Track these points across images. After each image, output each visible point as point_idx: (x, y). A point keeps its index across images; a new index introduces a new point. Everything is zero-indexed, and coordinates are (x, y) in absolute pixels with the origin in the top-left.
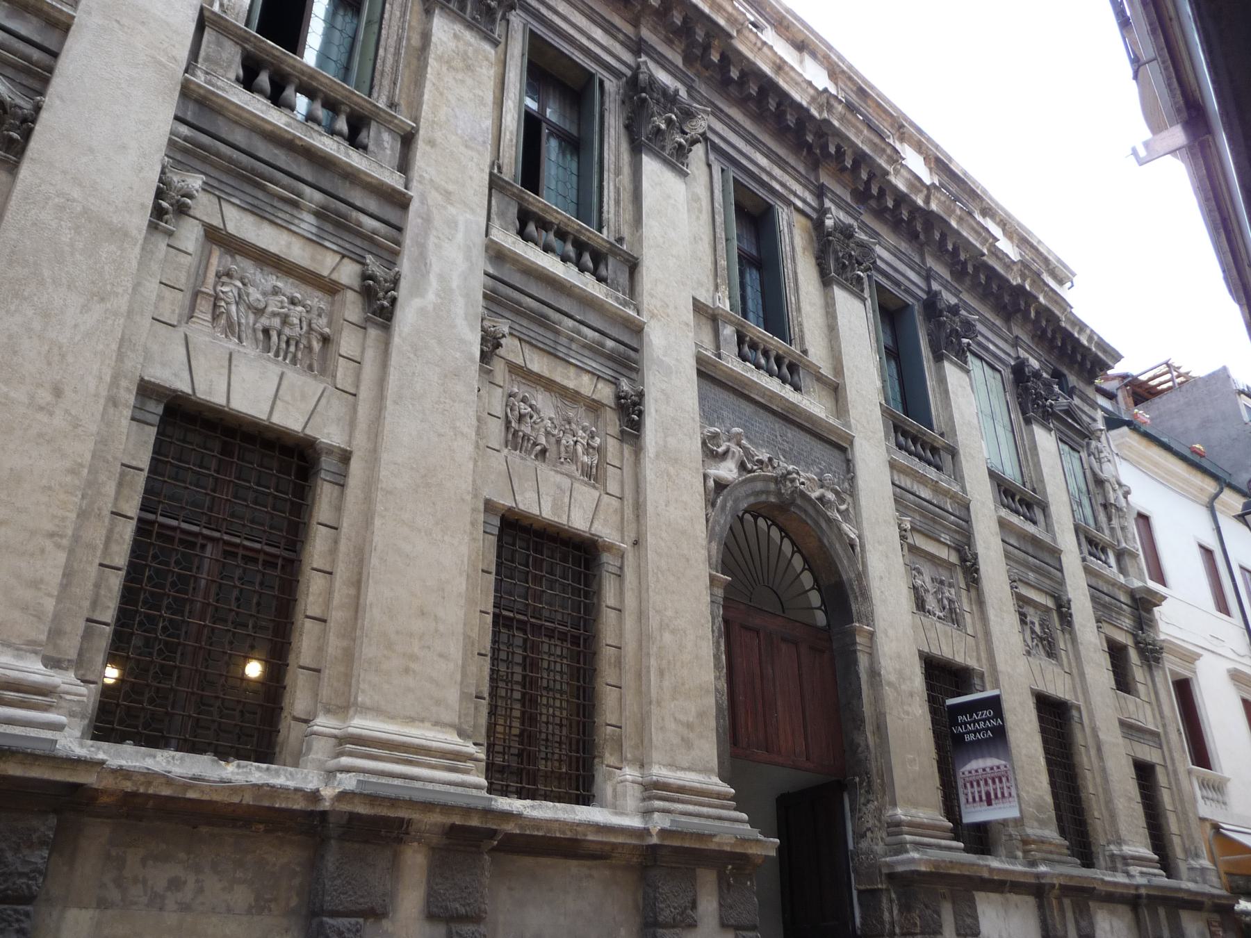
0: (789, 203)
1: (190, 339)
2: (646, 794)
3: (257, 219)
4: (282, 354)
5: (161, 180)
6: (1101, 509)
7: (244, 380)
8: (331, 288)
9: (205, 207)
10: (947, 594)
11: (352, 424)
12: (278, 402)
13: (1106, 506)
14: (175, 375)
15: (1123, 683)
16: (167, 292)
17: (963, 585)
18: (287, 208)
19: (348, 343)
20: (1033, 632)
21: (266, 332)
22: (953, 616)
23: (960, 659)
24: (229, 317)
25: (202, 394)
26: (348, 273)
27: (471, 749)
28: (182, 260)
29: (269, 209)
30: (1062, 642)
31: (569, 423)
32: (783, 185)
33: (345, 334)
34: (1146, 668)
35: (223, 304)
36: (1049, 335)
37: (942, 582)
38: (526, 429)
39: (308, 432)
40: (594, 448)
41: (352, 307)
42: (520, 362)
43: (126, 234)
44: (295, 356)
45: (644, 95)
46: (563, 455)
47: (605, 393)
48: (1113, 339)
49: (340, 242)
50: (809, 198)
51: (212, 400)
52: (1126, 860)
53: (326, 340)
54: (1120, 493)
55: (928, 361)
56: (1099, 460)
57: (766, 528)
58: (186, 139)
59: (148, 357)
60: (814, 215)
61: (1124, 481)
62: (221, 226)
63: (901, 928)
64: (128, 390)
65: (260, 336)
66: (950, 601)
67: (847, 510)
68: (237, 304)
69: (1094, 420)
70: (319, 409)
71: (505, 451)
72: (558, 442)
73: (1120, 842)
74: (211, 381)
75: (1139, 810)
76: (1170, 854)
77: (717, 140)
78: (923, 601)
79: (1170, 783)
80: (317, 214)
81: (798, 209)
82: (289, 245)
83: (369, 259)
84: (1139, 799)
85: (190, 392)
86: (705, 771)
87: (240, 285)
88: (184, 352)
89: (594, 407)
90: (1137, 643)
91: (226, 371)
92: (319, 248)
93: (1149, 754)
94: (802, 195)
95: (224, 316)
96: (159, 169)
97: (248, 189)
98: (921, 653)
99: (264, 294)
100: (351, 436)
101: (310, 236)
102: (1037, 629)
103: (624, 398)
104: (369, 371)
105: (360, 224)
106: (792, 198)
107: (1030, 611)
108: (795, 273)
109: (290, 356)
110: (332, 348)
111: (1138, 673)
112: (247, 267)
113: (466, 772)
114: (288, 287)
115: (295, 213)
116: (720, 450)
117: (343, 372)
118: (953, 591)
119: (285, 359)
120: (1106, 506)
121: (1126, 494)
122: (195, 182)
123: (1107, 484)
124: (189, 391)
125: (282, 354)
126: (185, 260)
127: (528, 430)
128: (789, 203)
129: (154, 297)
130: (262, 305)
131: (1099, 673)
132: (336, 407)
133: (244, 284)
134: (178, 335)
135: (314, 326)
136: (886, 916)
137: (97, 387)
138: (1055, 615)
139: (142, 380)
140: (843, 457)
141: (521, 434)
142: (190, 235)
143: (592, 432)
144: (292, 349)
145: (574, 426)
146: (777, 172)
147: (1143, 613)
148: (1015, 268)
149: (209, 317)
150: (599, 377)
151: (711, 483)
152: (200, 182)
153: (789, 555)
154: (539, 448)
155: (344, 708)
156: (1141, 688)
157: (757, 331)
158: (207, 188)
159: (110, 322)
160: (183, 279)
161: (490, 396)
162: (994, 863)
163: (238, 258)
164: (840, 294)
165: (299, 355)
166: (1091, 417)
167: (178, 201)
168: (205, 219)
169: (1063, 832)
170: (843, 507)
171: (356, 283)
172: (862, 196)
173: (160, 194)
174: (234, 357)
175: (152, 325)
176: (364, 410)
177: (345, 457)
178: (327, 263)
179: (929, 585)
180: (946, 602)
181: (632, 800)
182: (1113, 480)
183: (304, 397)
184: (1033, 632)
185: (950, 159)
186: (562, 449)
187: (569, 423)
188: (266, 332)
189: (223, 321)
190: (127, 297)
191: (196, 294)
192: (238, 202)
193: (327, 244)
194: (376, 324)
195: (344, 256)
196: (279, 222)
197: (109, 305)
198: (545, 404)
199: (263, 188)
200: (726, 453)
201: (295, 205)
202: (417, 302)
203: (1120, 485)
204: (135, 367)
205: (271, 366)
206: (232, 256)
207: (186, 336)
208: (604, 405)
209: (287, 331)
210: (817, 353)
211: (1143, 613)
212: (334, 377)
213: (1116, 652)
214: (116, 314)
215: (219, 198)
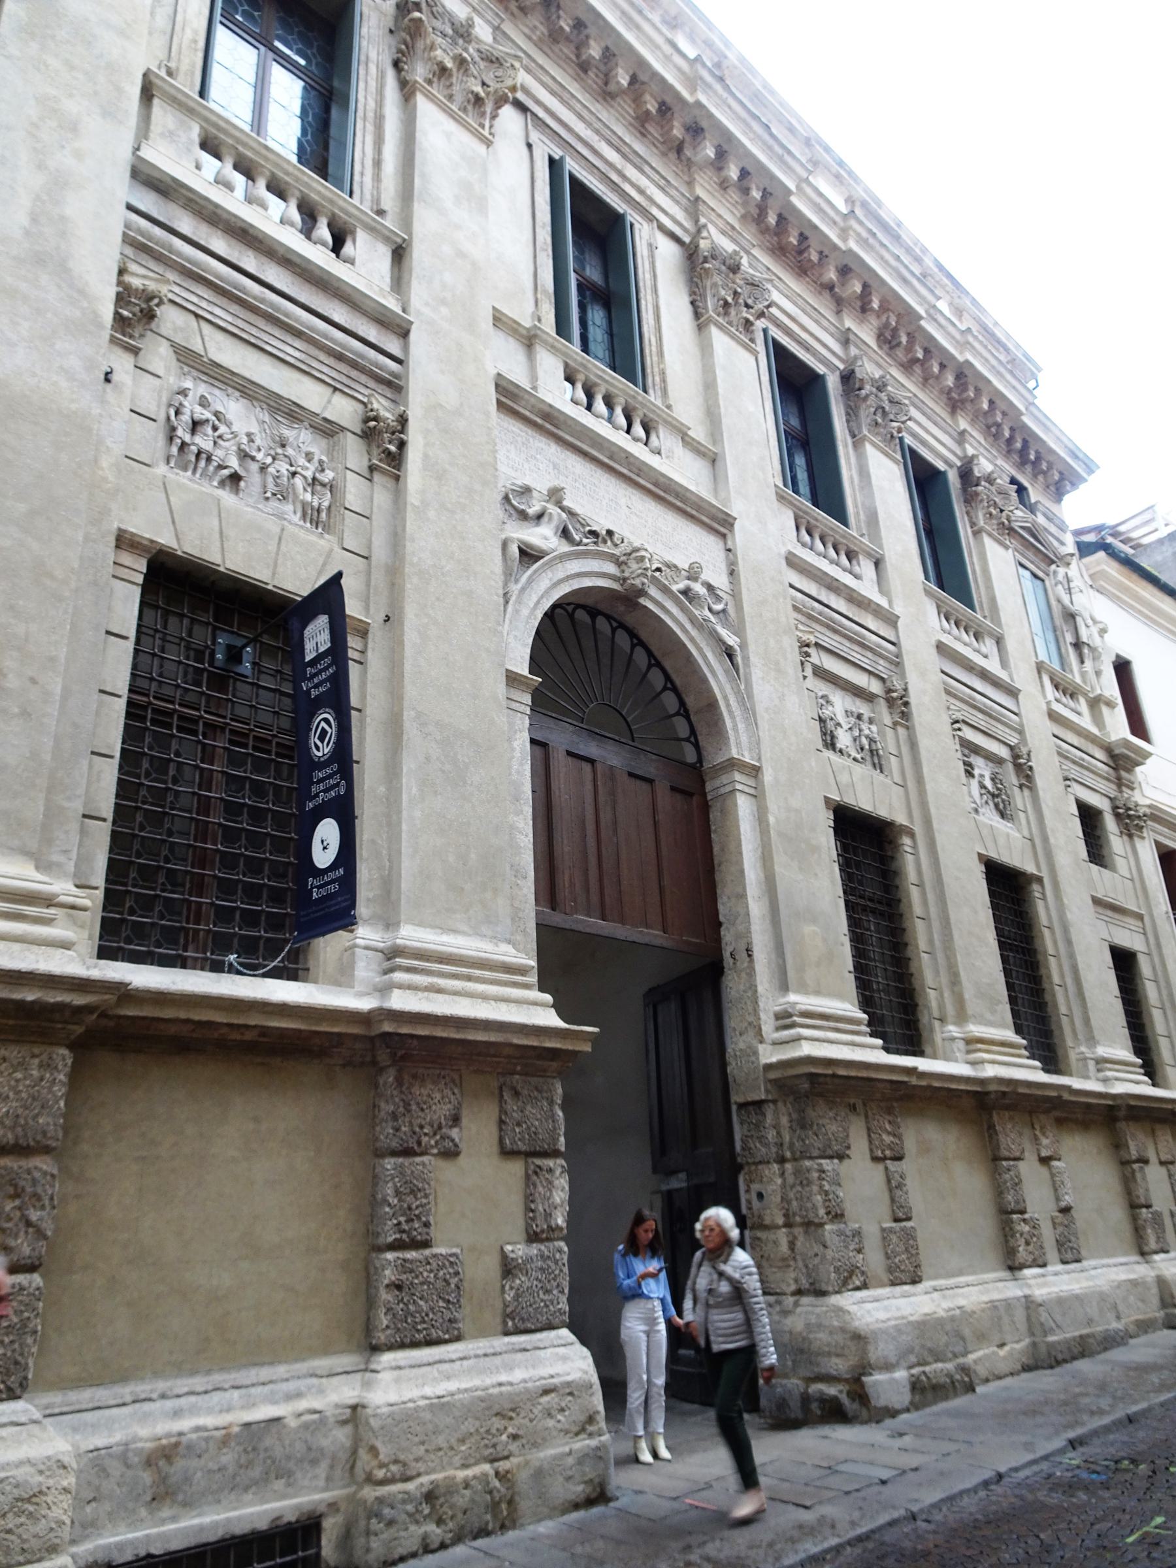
0: (651, 218)
2: (387, 965)
6: (1071, 650)
10: (867, 732)
13: (1078, 645)
15: (1097, 852)
17: (887, 720)
20: (982, 786)
22: (874, 757)
23: (883, 812)
27: (63, 888)
30: (1020, 799)
31: (283, 446)
32: (641, 192)
34: (1125, 838)
36: (1007, 434)
37: (859, 717)
38: (203, 441)
40: (324, 485)
42: (197, 347)
45: (417, 14)
46: (271, 486)
47: (343, 410)
48: (1087, 447)
50: (680, 215)
52: (1101, 1062)
54: (1094, 630)
55: (846, 446)
56: (1069, 591)
57: (608, 631)
60: (687, 239)
61: (1098, 618)
63: (793, 1153)
66: (872, 741)
67: (724, 611)
69: (1062, 543)
71: (162, 469)
72: (263, 469)
73: (1092, 1041)
75: (1118, 1006)
76: (1155, 1059)
77: (541, 114)
78: (833, 737)
79: (1155, 974)
81: (662, 228)
84: (1117, 992)
86: (1003, 1026)
89: (328, 429)
90: (1115, 808)
93: (1129, 939)
94: (671, 210)
98: (827, 800)
102: (988, 783)
103: (375, 419)
106: (655, 211)
107: (979, 763)
108: (657, 308)
109: (199, 471)
111: (1116, 842)
113: (47, 922)
116: (531, 511)
118: (874, 728)
120: (1078, 645)
121: (1103, 631)
123: (1078, 619)
127: (207, 445)
128: (651, 218)
131: (1068, 836)
136: (771, 1135)
138: (1010, 766)
140: (721, 544)
141: (194, 449)
143: (321, 462)
145: (290, 451)
146: (631, 172)
147: (1123, 773)
148: (878, 1096)
150: (336, 389)
151: (514, 550)
153: (659, 689)
154: (226, 472)
155: (962, 1017)
156: (1120, 863)
157: (598, 369)
162: (922, 1064)
164: (719, 340)
166: (1058, 539)
169: (1018, 1030)
170: (718, 607)
172: (757, 218)
179: (841, 718)
180: (865, 742)
181: (366, 969)
182: (1087, 616)
184: (982, 786)
185: (879, 204)
186: (270, 480)
187: (283, 446)
198: (241, 417)
200: (540, 516)
203: (1095, 622)
208: (343, 429)
210: (685, 406)
211: (1123, 773)
213: (1088, 816)
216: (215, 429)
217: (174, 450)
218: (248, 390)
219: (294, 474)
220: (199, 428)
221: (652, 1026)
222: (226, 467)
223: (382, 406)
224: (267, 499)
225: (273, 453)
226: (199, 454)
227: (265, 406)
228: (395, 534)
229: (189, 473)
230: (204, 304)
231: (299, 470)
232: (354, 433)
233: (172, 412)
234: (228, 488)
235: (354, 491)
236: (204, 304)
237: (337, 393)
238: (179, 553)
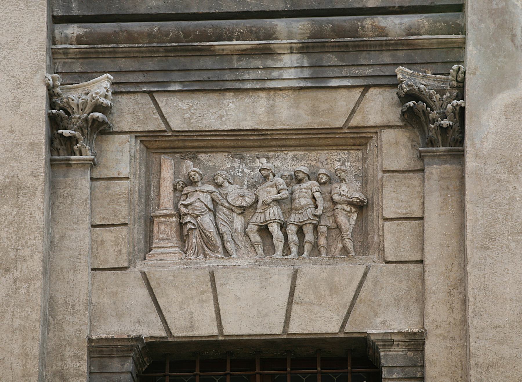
1: (150, 276)
3: (214, 97)
4: (294, 249)
5: (52, 105)
7: (237, 297)
8: (357, 138)
9: (133, 113)
11: (421, 300)
12: (295, 307)
14: (139, 322)
16: (105, 235)
18: (257, 63)
19: (394, 199)
21: (264, 230)
24: (203, 233)
25: (181, 330)
26: (379, 107)
28: (117, 190)
29: (228, 76)
33: (387, 190)
35: (188, 219)
39: (348, 328)
41: (396, 149)
43: (19, 187)
44: (316, 246)
49: (355, 71)
51: (196, 334)
53: (361, 207)
58: (79, 40)
59: (95, 315)
62: (163, 127)
64: (76, 357)
65: (256, 238)
68: (214, 212)
70: (362, 295)
74: (191, 313)
80: (305, 49)
82: (271, 110)
83: (402, 72)
85: (163, 334)
87: (212, 188)
88: (146, 292)
91: (211, 295)
92: (321, 94)
95: (196, 233)
96: (43, 92)
97: (186, 62)
99: (253, 186)
100: (422, 314)
101: (302, 84)
104: (438, 224)
105: (383, 31)
109: (307, 247)
110: (374, 215)
112: (221, 162)
114: (285, 163)
115: (270, 63)
117: (395, 240)
119: (300, 252)
122: (100, 86)
124: (159, 332)
125: (294, 249)
126: (122, 187)
129: (86, 245)
130: (248, 201)
132: (389, 284)
133: (219, 186)
134: (133, 276)
135: (336, 197)
137: (24, 365)
139: (90, 340)
142: (121, 156)
144: (309, 237)
149: (174, 241)
152: (107, 84)
158: (118, 89)
159: (23, 291)
160: (124, 211)
161: (381, 132)
163: (203, 157)
165: (322, 241)
167: (86, 120)
168: (137, 128)
171: (394, 116)
173: (54, 122)
174: (216, 276)
175: (93, 277)
176: (436, 280)
177: (416, 342)
178: (337, 107)
183: (334, 289)
188: (264, 230)
189: (195, 239)
190: (38, 257)
191: (150, 221)
192: (177, 87)
193: (334, 83)
194: (441, 158)
195: (367, 88)
196: (248, 85)
197: (17, 274)
199: (210, 52)
201: (267, 52)
202: (503, 99)
204: (77, 330)
205: (275, 269)
206: (194, 158)
207: (144, 274)
209: (294, 218)
212: (381, 249)
214: (28, 280)
215: (150, 93)
223: (423, 81)
237: (372, 91)
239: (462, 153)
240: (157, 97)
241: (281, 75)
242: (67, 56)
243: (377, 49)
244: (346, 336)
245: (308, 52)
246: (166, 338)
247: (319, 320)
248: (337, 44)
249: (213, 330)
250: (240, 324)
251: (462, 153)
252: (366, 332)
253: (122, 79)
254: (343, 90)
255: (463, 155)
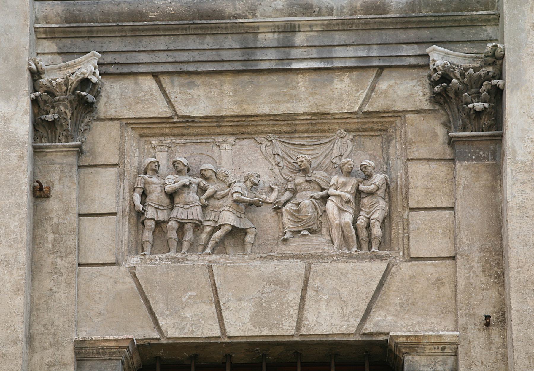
26: (406, 91)
38: (189, 209)
89: (377, 124)
109: (186, 245)
141: (173, 224)
215: (155, 75)
216: (202, 190)
217: (148, 235)
218: (242, 126)
219: (325, 199)
220: (177, 200)
221: (349, 64)
222: (219, 228)
224: (285, 240)
225: (290, 186)
226: (181, 226)
227: (273, 137)
228: (232, 134)
229: (172, 253)
230: (163, 57)
231: (332, 191)
232: (419, 112)
233: (137, 198)
234: (230, 249)
235: (424, 179)
236: (163, 57)
237: (385, 72)
238: (163, 341)
239: (500, 138)
240: (162, 78)
241: (289, 54)
242: (460, 23)
243: (360, 28)
244: (365, 338)
245: (52, 38)
246: (159, 339)
247: (330, 318)
248: (452, 18)
249: (216, 332)
250: (242, 324)
251: (500, 138)
252: (388, 334)
253: (109, 59)
254: (168, 65)
255: (501, 140)
